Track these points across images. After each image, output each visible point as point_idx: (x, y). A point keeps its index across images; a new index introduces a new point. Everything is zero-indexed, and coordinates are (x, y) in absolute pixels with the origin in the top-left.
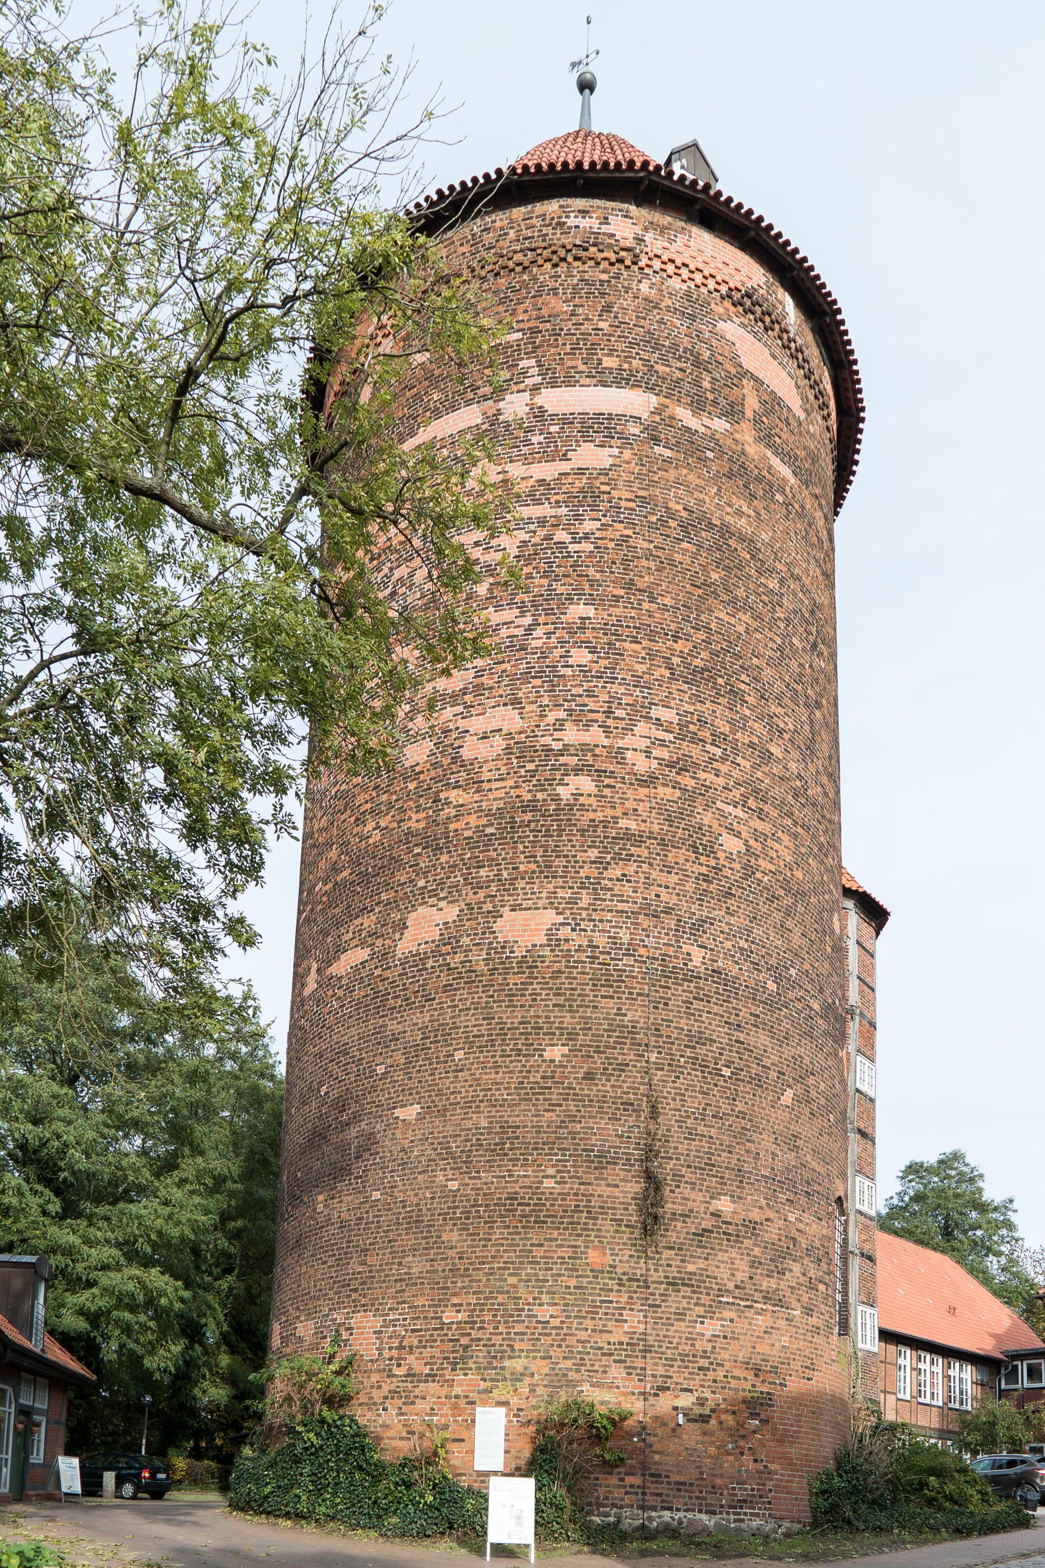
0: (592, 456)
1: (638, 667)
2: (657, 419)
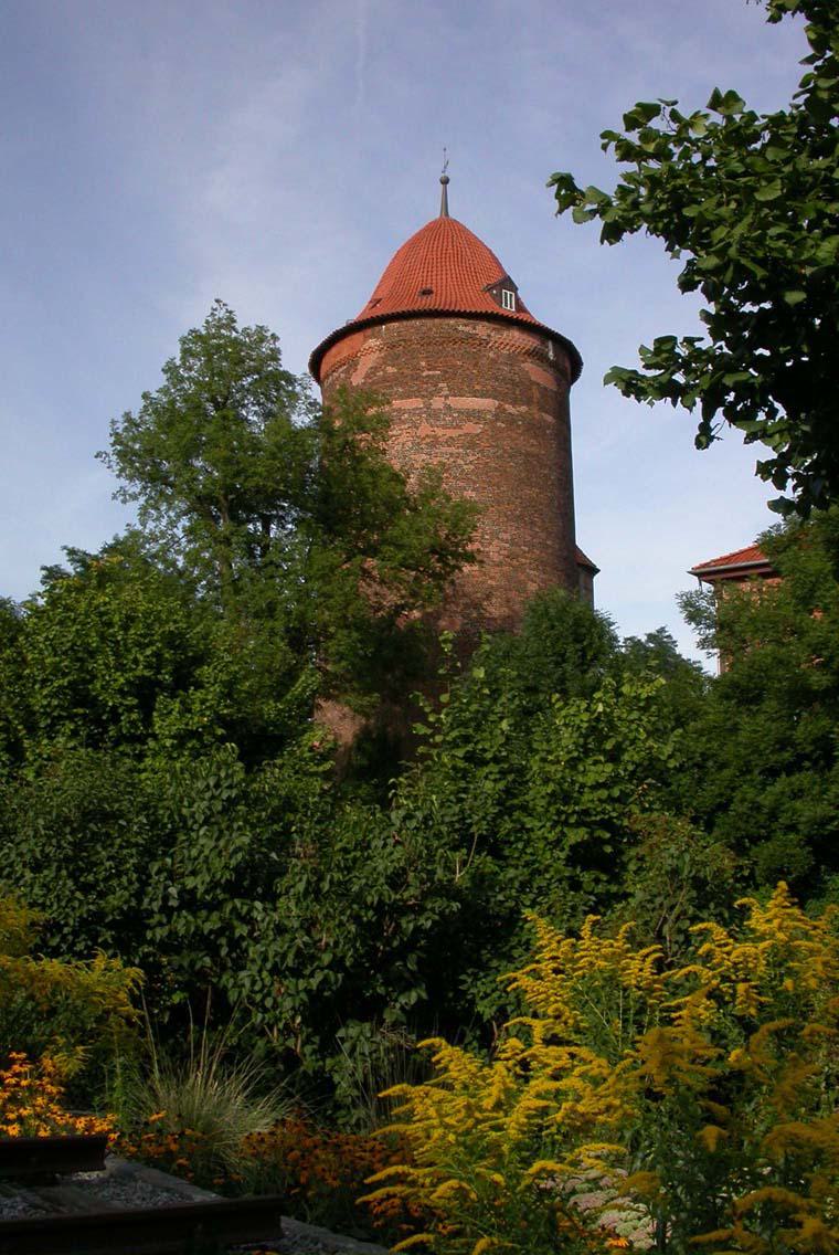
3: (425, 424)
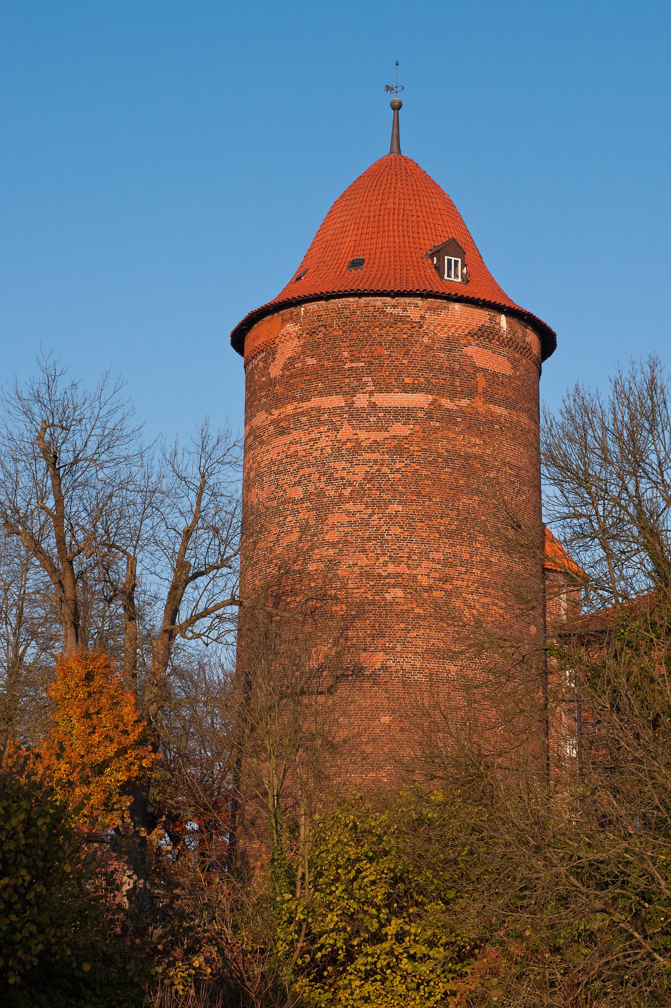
0: (400, 429)
1: (423, 534)
2: (432, 407)
3: (346, 425)
